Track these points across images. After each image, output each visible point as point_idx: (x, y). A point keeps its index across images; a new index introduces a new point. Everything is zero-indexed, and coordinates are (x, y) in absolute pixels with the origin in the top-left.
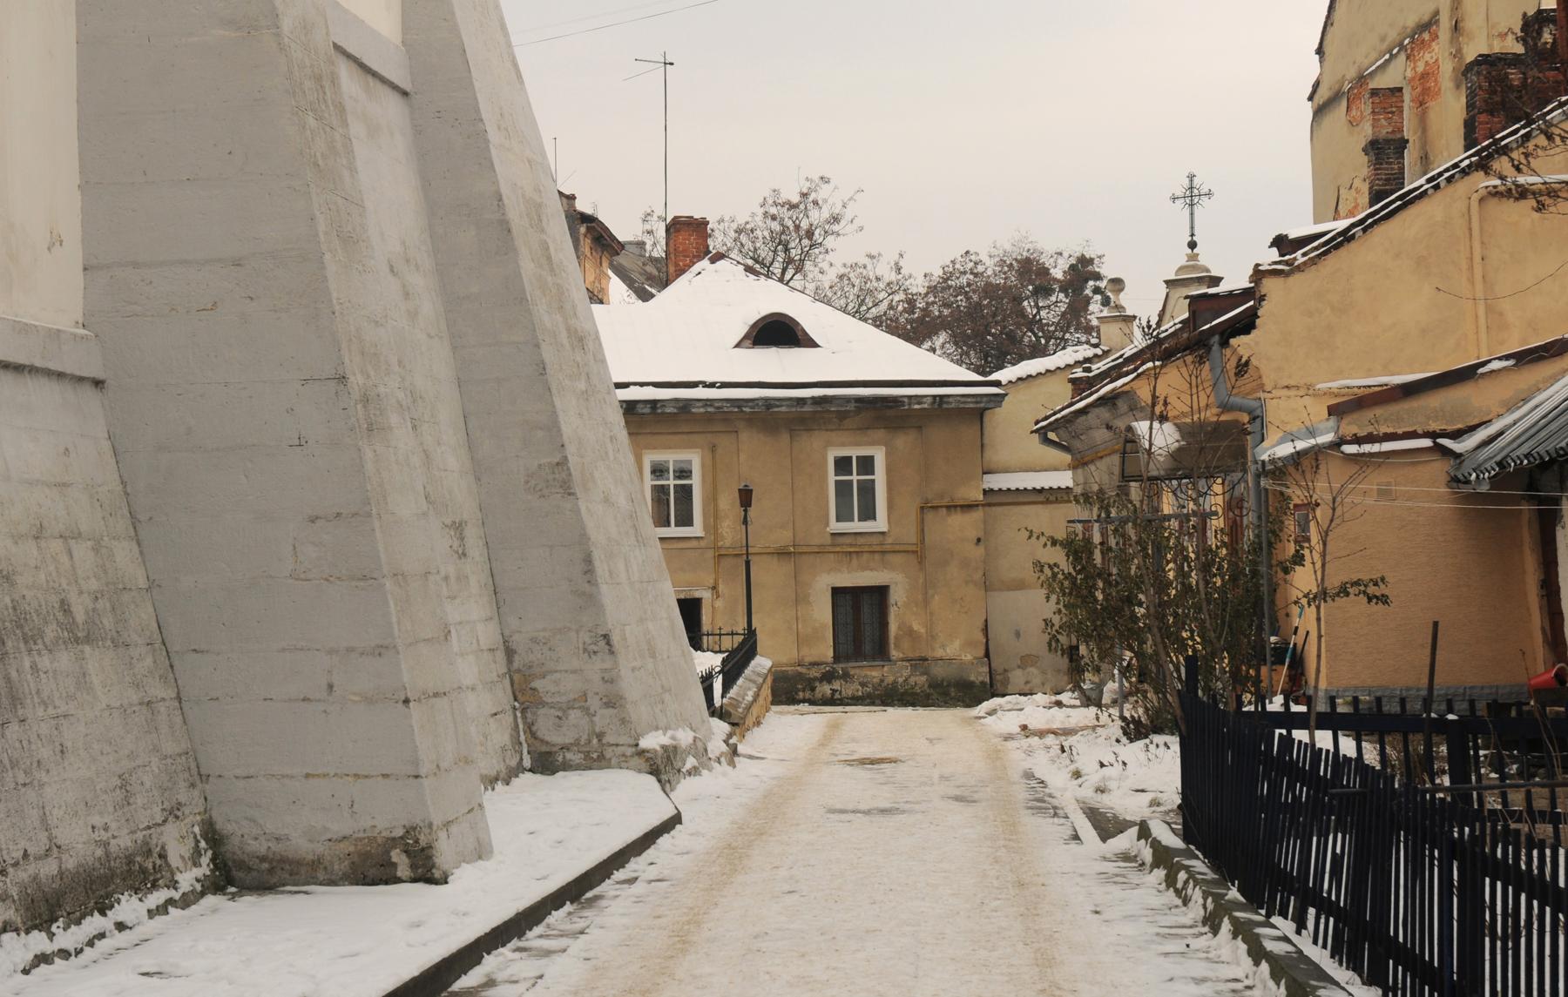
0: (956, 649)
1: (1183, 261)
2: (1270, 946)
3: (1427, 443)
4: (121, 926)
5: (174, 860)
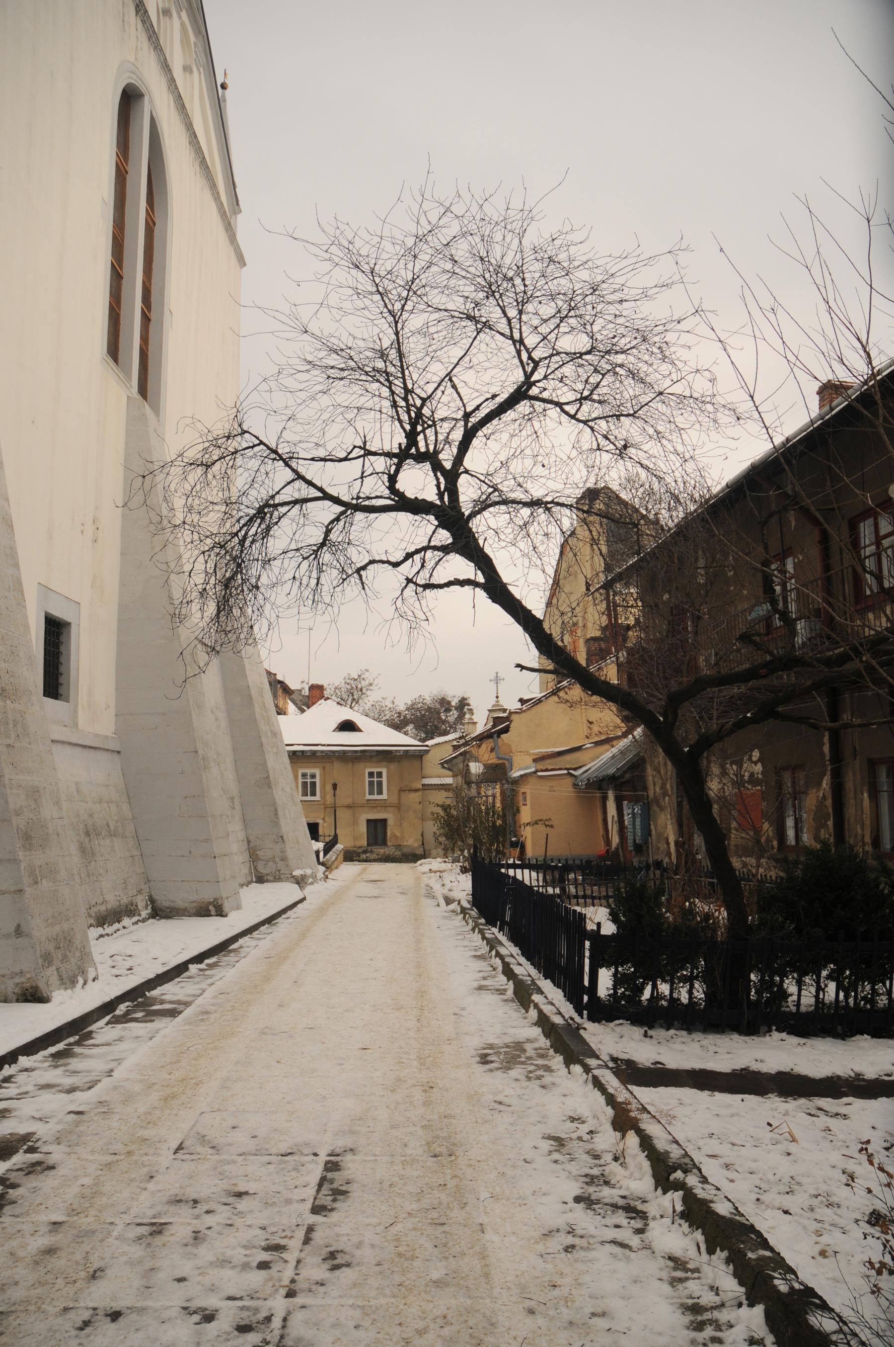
0: (412, 842)
1: (494, 703)
2: (487, 935)
3: (565, 772)
4: (124, 927)
5: (140, 907)
